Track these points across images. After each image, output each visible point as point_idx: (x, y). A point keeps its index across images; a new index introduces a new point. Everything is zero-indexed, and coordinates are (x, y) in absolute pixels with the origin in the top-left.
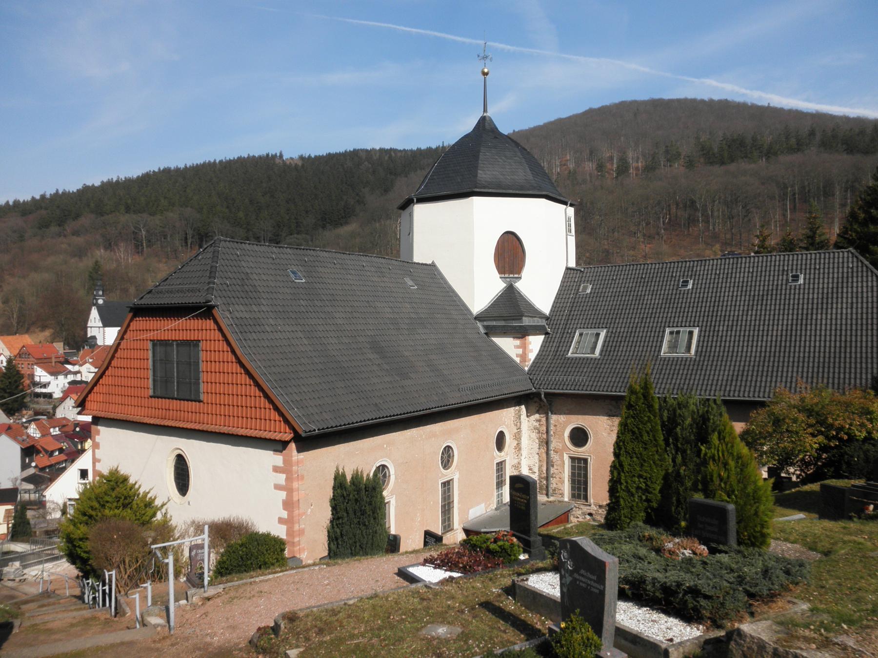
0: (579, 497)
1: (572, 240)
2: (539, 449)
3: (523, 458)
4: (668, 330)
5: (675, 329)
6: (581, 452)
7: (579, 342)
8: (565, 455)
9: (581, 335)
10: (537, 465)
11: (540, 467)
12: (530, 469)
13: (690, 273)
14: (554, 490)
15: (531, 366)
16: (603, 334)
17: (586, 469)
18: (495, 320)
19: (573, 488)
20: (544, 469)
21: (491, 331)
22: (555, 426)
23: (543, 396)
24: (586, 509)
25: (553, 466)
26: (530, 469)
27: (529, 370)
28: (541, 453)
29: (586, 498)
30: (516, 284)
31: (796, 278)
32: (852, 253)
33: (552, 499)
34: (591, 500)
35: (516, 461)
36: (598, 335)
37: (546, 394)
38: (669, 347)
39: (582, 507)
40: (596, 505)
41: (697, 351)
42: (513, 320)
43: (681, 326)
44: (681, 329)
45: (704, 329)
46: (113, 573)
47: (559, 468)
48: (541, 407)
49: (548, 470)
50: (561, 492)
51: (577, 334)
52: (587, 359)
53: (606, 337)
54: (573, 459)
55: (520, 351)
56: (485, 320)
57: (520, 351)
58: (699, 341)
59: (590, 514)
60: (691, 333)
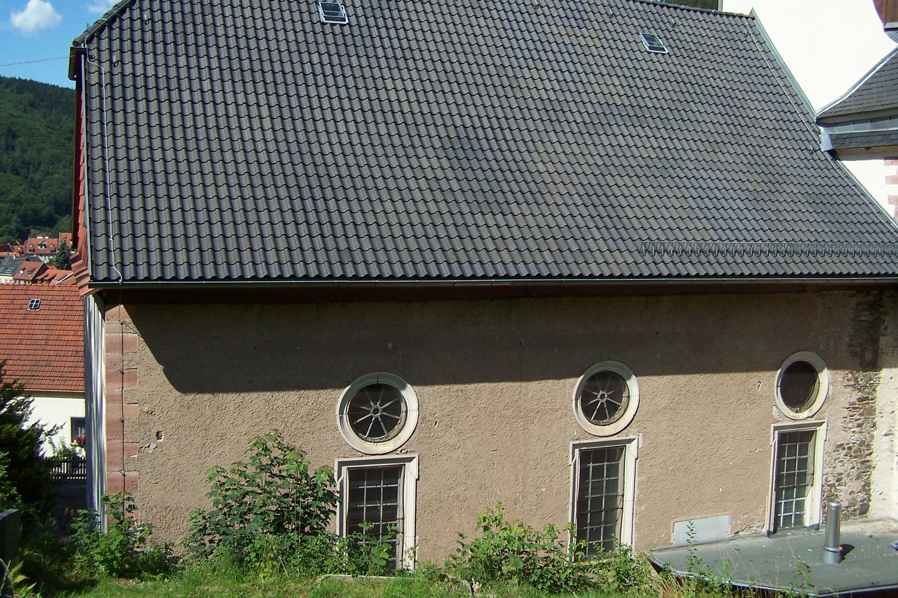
35: (852, 438)
42: (890, 118)
56: (836, 124)
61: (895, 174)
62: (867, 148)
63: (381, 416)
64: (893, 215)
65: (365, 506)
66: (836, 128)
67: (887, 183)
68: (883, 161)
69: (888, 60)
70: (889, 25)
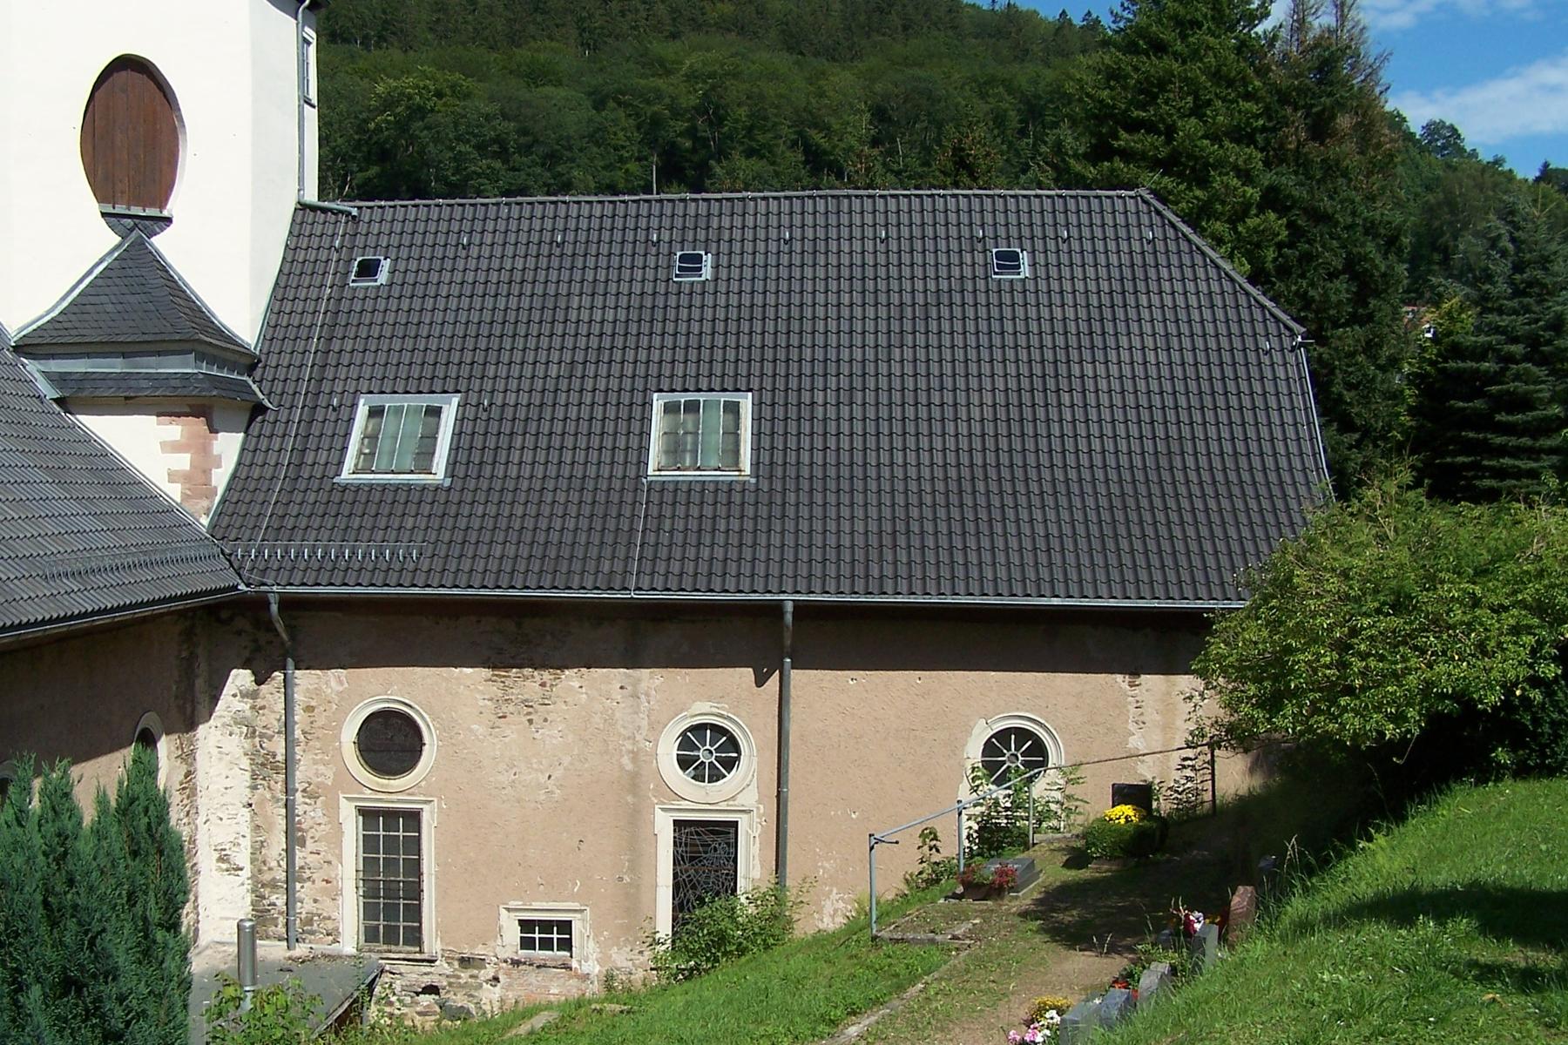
0: (391, 937)
1: (312, 115)
2: (254, 788)
3: (200, 821)
4: (658, 402)
5: (683, 398)
6: (395, 791)
7: (371, 438)
8: (343, 802)
9: (376, 412)
10: (246, 844)
11: (258, 848)
12: (221, 859)
13: (701, 235)
14: (310, 922)
15: (220, 514)
16: (450, 409)
17: (415, 845)
18: (88, 355)
19: (369, 912)
20: (278, 842)
21: (79, 394)
22: (309, 709)
23: (274, 608)
24: (416, 975)
25: (303, 845)
26: (221, 859)
27: (213, 526)
28: (262, 802)
29: (415, 937)
30: (154, 240)
31: (1009, 261)
32: (1145, 201)
33: (301, 950)
34: (432, 943)
36: (435, 412)
37: (288, 603)
38: (667, 452)
39: (403, 968)
40: (449, 961)
41: (756, 464)
42: (159, 354)
43: (699, 390)
44: (701, 397)
45: (767, 398)
46: (346, 475)
47: (322, 847)
48: (258, 649)
49: (289, 853)
50: (330, 925)
51: (362, 411)
52: (409, 488)
53: (460, 420)
54: (369, 815)
55: (183, 461)
56: (53, 356)
57: (183, 461)
58: (757, 435)
59: (432, 989)
60: (733, 409)
61: (178, 437)
62: (127, 398)
63: (703, 762)
64: (179, 501)
65: (537, 936)
66: (51, 361)
67: (163, 451)
68: (155, 418)
69: (109, 260)
70: (109, 209)
